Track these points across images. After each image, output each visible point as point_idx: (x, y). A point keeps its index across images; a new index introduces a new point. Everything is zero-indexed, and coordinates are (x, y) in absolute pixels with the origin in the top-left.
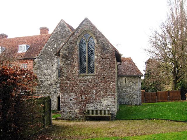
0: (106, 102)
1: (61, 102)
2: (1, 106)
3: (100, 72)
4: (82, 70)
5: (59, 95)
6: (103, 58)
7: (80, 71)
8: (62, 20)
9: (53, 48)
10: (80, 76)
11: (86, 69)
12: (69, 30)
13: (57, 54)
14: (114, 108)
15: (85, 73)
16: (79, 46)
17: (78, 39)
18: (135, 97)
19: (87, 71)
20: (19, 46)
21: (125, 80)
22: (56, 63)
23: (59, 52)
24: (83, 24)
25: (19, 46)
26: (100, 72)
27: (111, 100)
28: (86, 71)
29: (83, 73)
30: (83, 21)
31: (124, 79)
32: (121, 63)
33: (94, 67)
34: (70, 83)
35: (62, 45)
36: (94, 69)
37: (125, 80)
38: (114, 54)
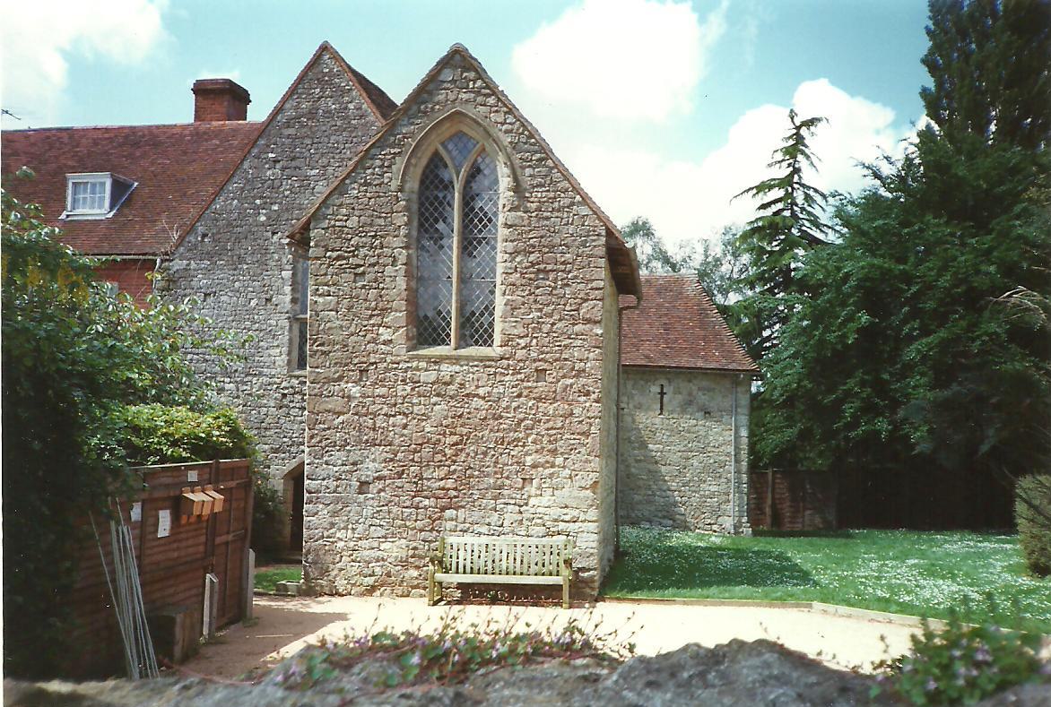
0: (545, 500)
1: (306, 495)
2: (1050, 63)
3: (522, 342)
4: (426, 331)
5: (294, 463)
6: (542, 266)
7: (420, 334)
8: (325, 48)
9: (275, 207)
10: (419, 358)
11: (449, 324)
12: (366, 106)
13: (298, 236)
14: (587, 541)
15: (443, 342)
16: (415, 197)
17: (413, 161)
18: (713, 488)
19: (453, 334)
20: (72, 178)
21: (662, 394)
22: (288, 289)
23: (306, 228)
24: (442, 77)
25: (72, 178)
26: (522, 342)
27: (576, 493)
28: (448, 335)
29: (476, 343)
30: (444, 63)
31: (656, 389)
32: (639, 299)
33: (492, 314)
34: (364, 396)
35: (322, 189)
36: (491, 325)
37: (662, 394)
38: (602, 251)
